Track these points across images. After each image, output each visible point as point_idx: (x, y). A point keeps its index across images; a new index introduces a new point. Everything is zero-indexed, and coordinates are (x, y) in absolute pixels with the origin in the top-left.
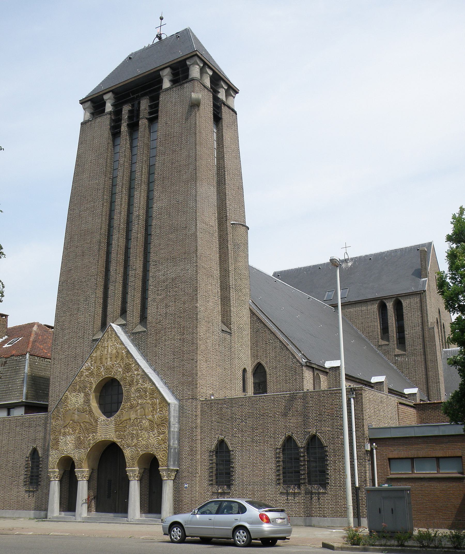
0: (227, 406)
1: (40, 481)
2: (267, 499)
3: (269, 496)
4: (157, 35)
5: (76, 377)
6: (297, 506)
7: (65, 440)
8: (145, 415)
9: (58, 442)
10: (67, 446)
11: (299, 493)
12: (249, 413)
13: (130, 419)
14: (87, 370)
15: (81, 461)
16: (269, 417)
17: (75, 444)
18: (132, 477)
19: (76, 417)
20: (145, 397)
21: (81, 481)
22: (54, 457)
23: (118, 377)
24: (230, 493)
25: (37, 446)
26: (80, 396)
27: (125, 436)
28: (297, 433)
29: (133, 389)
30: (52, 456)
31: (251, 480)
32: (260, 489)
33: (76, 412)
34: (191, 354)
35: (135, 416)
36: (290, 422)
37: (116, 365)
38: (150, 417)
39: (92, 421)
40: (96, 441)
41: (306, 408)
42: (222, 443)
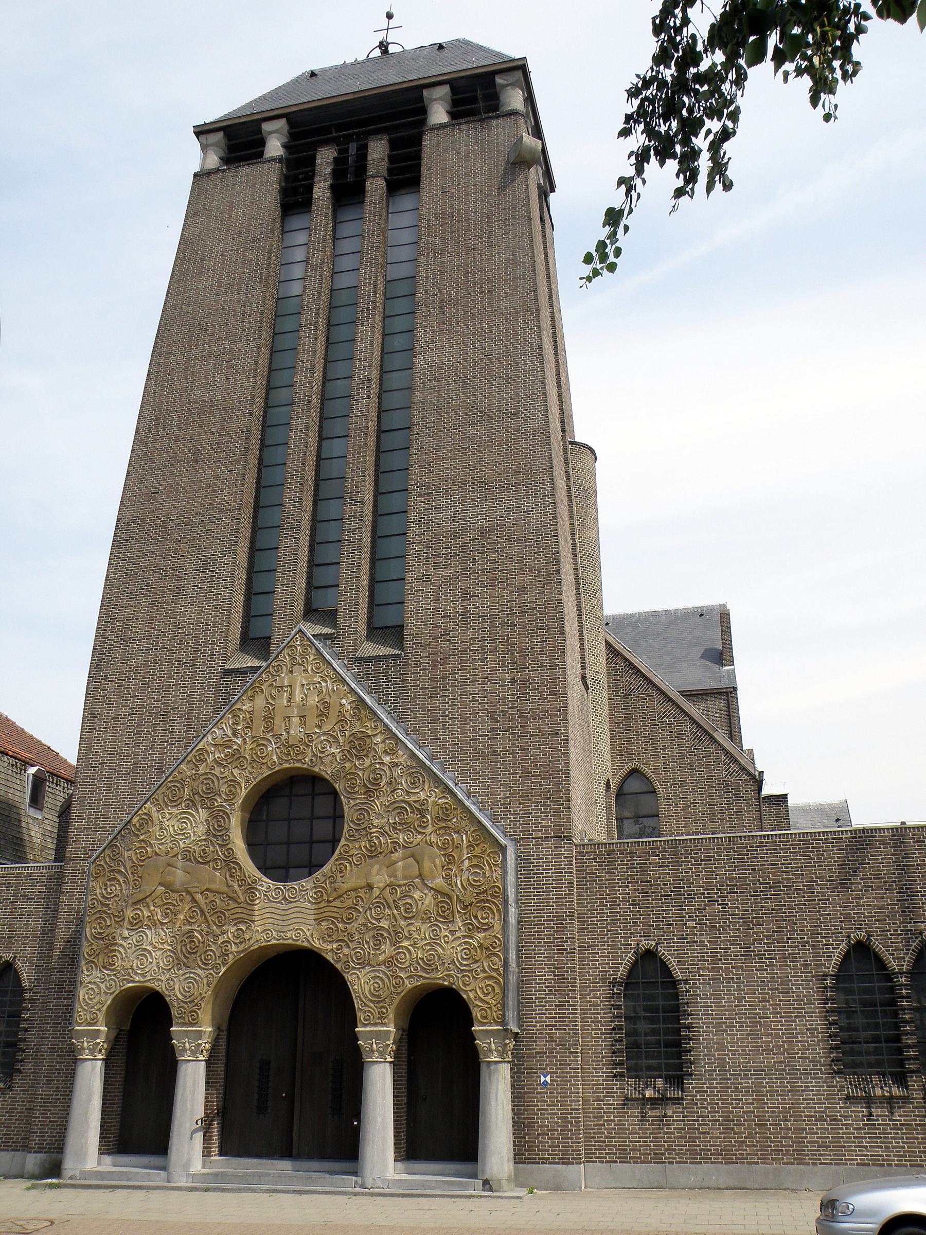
0: (659, 859)
1: (22, 1061)
2: (805, 1116)
3: (811, 1108)
4: (381, 43)
6: (903, 1134)
7: (138, 942)
8: (420, 876)
9: (112, 945)
10: (146, 956)
11: (906, 1099)
12: (731, 879)
13: (370, 887)
15: (193, 1003)
16: (795, 890)
17: (174, 953)
18: (376, 1054)
19: (179, 876)
20: (419, 826)
22: (97, 990)
23: (326, 770)
24: (682, 1099)
25: (15, 957)
26: (193, 816)
27: (351, 935)
28: (881, 935)
29: (378, 804)
30: (90, 986)
31: (749, 1063)
32: (780, 1087)
33: (180, 862)
34: (548, 721)
36: (858, 906)
37: (319, 736)
38: (439, 882)
39: (236, 888)
40: (251, 946)
41: (904, 869)
42: (648, 957)
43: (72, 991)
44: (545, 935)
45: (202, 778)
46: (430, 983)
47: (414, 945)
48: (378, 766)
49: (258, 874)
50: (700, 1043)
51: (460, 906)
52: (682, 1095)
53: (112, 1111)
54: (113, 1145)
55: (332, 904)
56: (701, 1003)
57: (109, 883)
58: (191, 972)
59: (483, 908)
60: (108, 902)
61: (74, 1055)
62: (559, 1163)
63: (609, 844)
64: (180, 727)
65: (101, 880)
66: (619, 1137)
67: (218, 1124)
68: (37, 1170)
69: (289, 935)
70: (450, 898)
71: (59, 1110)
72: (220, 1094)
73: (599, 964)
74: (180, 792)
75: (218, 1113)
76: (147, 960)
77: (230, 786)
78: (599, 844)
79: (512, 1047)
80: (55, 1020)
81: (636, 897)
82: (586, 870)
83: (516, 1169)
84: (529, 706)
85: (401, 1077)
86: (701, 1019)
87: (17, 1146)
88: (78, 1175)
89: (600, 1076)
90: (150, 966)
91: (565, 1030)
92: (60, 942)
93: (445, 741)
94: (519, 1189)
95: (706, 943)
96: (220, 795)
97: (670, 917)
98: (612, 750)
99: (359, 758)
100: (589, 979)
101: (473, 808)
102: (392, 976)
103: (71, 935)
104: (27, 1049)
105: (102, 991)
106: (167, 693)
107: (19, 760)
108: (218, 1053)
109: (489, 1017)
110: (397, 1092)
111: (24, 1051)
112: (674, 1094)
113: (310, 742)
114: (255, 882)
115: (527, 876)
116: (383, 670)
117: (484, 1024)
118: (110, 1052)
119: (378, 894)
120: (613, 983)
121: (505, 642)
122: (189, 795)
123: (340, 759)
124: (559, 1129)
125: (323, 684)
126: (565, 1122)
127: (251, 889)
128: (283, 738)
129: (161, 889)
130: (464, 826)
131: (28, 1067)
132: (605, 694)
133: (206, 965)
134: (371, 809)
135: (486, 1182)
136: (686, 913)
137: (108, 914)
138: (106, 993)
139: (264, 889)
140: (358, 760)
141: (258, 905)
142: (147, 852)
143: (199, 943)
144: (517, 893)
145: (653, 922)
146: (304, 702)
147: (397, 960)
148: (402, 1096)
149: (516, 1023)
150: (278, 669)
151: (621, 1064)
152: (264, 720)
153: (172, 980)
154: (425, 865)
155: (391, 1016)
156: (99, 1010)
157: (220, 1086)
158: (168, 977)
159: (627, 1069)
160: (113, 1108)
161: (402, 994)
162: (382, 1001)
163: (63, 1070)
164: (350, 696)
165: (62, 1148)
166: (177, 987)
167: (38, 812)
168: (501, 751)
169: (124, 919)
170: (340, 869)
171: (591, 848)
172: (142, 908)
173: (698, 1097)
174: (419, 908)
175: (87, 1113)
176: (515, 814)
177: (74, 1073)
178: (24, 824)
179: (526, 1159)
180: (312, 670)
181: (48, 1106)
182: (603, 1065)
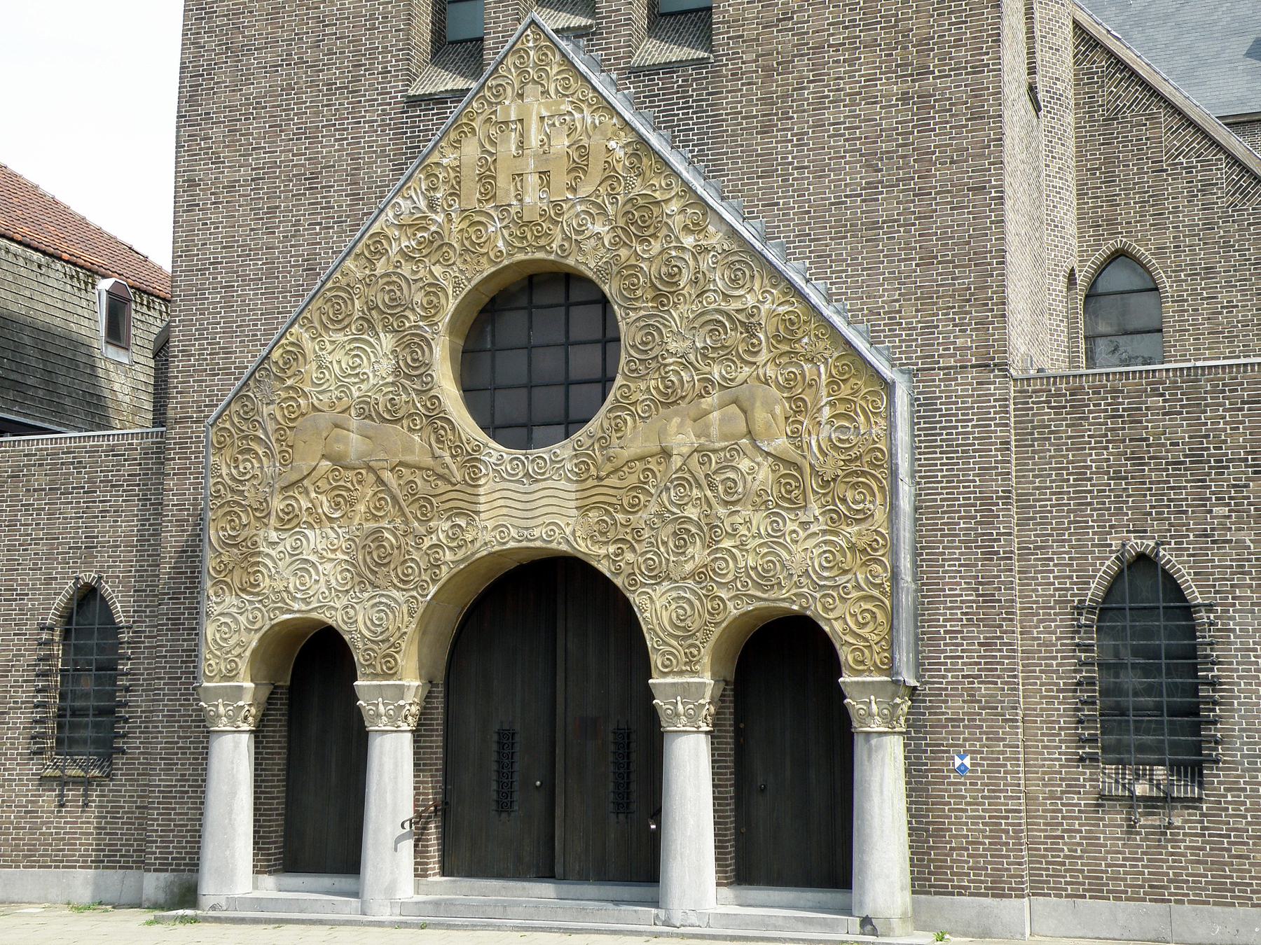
0: (1165, 401)
1: (124, 736)
5: (344, 259)
9: (253, 555)
13: (666, 453)
14: (409, 232)
15: (389, 645)
19: (354, 443)
20: (747, 351)
21: (389, 735)
22: (233, 626)
23: (587, 262)
24: (1200, 800)
25: (100, 578)
26: (372, 346)
27: (638, 531)
30: (223, 620)
33: (354, 422)
37: (573, 206)
38: (781, 444)
39: (448, 459)
43: (194, 629)
44: (960, 529)
47: (742, 546)
48: (674, 253)
49: (482, 437)
50: (1233, 710)
52: (1200, 794)
53: (271, 810)
54: (275, 860)
56: (1236, 643)
58: (383, 595)
59: (855, 486)
60: (241, 488)
61: (204, 726)
62: (986, 895)
63: (1075, 376)
64: (339, 199)
65: (228, 452)
66: (1088, 858)
67: (436, 827)
68: (161, 897)
69: (537, 533)
70: (799, 468)
71: (188, 809)
72: (437, 782)
73: (1055, 577)
74: (346, 307)
75: (436, 811)
77: (428, 294)
78: (1055, 378)
79: (906, 710)
80: (168, 737)
81: (1120, 466)
82: (1032, 421)
83: (914, 902)
84: (934, 140)
85: (725, 755)
86: (1237, 670)
87: (128, 862)
88: (223, 903)
89: (1056, 759)
90: (317, 587)
91: (996, 683)
92: (170, 552)
94: (921, 933)
95: (1248, 543)
96: (413, 310)
97: (1182, 500)
98: (1081, 218)
99: (643, 240)
100: (1037, 602)
101: (838, 321)
102: (707, 596)
103: (187, 541)
104: (130, 717)
105: (243, 627)
106: (314, 140)
107: (82, 267)
108: (432, 719)
109: (868, 662)
110: (719, 779)
111: (126, 721)
112: (1186, 792)
113: (558, 215)
114: (477, 449)
115: (930, 432)
116: (679, 87)
117: (859, 673)
118: (261, 720)
119: (679, 464)
120: (1079, 609)
121: (893, 27)
122: (363, 311)
124: (987, 841)
125: (577, 115)
126: (997, 830)
127: (472, 461)
128: (513, 211)
129: (326, 464)
131: (134, 744)
132: (1070, 119)
134: (665, 326)
135: (866, 921)
136: (1213, 493)
137: (243, 506)
138: (248, 630)
139: (492, 460)
140: (641, 242)
141: (486, 485)
143: (393, 549)
144: (914, 460)
145: (1152, 507)
147: (713, 570)
148: (726, 786)
149: (912, 673)
150: (499, 91)
151: (1092, 740)
152: (480, 180)
153: (353, 607)
155: (706, 660)
156: (239, 656)
157: (437, 770)
159: (1103, 748)
160: (272, 804)
161: (724, 625)
163: (189, 748)
164: (622, 134)
165: (197, 865)
166: (360, 619)
167: (122, 352)
168: (884, 222)
169: (269, 514)
171: (1042, 384)
172: (297, 495)
173: (1230, 798)
174: (748, 486)
175: (231, 812)
176: (910, 329)
177: (207, 753)
178: (101, 373)
179: (930, 886)
180: (557, 91)
181: (171, 803)
182: (1060, 741)
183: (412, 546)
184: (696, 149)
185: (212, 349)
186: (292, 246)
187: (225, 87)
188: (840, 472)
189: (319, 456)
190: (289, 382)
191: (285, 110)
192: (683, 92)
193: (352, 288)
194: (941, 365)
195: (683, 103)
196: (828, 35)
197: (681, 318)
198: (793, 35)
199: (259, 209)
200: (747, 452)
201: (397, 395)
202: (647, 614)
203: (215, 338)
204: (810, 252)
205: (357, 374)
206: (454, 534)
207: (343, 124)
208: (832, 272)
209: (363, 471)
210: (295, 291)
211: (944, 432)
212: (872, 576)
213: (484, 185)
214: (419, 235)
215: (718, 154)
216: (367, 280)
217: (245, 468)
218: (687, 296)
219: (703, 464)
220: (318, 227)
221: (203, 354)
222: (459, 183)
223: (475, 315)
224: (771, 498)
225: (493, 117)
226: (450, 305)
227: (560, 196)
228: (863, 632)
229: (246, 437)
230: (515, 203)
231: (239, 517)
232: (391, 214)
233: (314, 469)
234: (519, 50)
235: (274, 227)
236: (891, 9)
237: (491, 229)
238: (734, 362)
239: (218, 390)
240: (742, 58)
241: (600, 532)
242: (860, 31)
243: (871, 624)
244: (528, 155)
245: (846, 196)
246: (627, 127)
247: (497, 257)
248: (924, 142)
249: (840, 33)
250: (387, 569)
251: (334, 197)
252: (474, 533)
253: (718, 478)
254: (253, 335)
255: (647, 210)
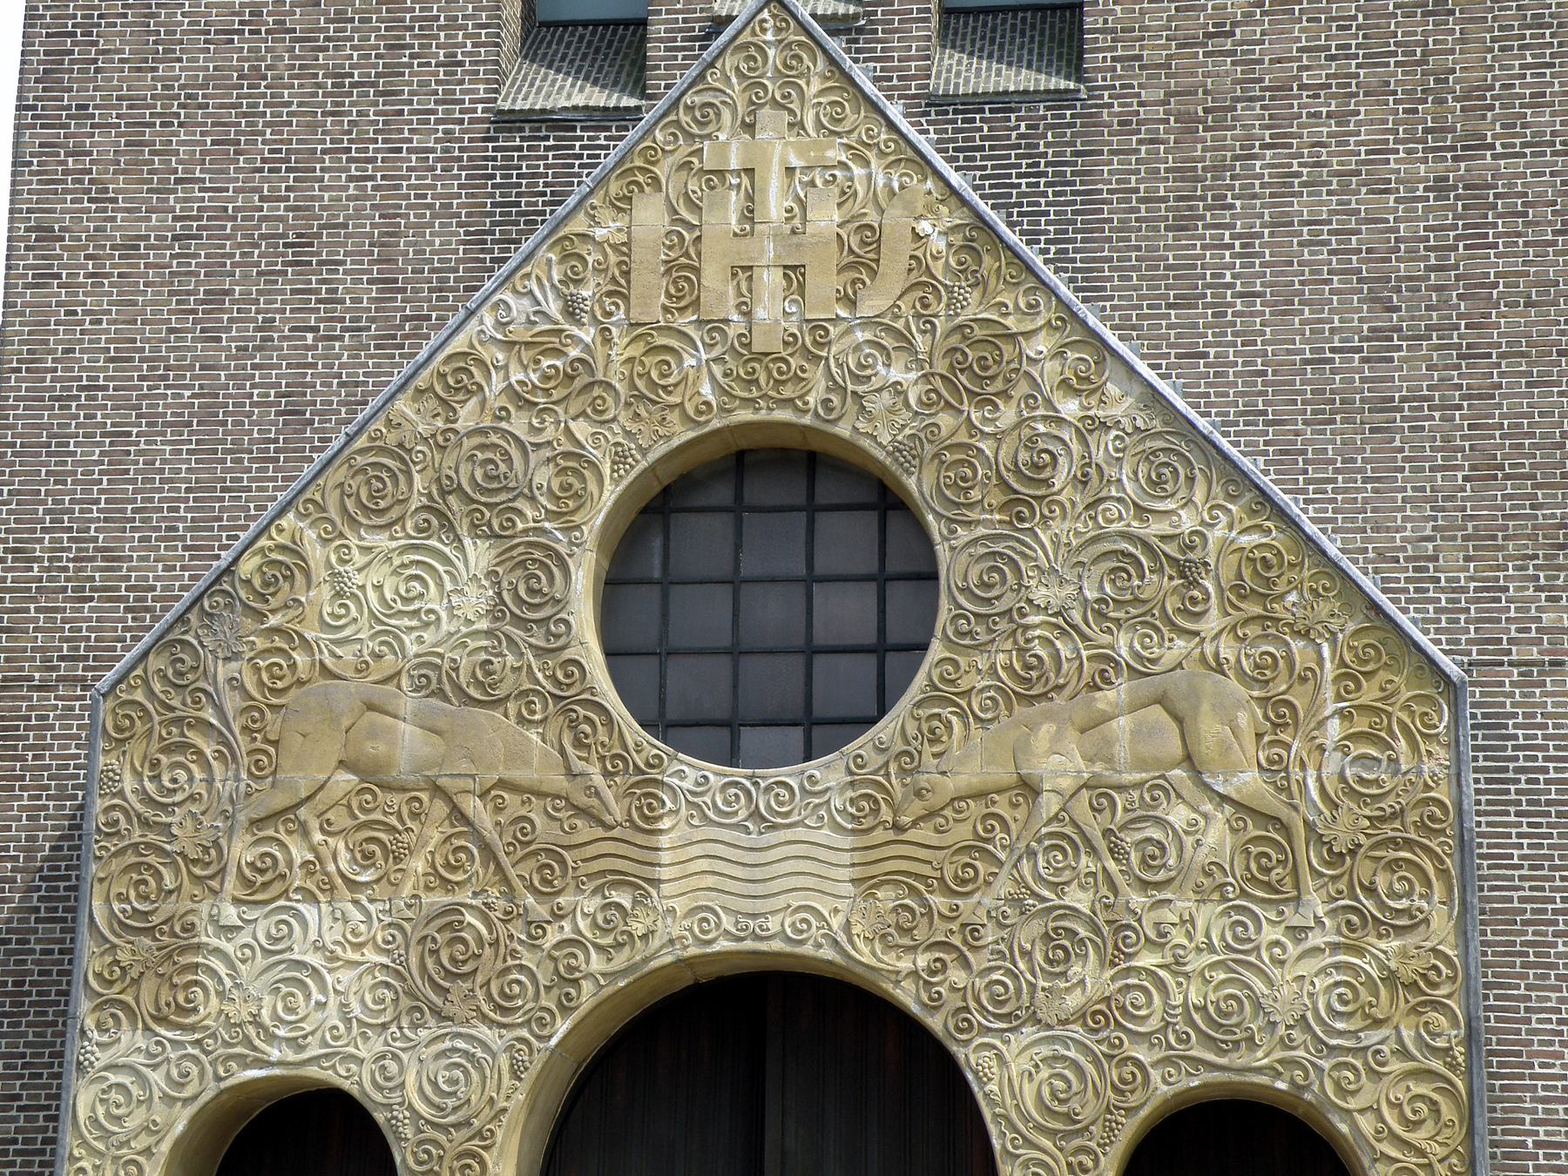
5: (392, 397)
8: (1189, 759)
9: (183, 950)
13: (1029, 788)
14: (526, 355)
22: (136, 1091)
26: (446, 560)
27: (972, 931)
30: (113, 1078)
33: (408, 702)
35: (1082, 764)
37: (849, 331)
38: (1248, 782)
39: (598, 780)
45: (468, 443)
46: (1230, 1083)
48: (1041, 428)
51: (1322, 859)
55: (910, 835)
57: (164, 759)
60: (164, 819)
65: (136, 749)
69: (773, 924)
70: (1285, 829)
76: (308, 996)
77: (563, 471)
84: (1494, 264)
90: (319, 1015)
93: (1222, 362)
96: (532, 499)
102: (1110, 1057)
105: (157, 1094)
106: (304, 172)
113: (821, 345)
116: (1020, 136)
119: (1055, 809)
121: (1418, 63)
122: (430, 496)
123: (920, 401)
125: (858, 171)
128: (732, 332)
129: (346, 780)
130: (1324, 615)
133: (505, 1011)
138: (169, 1100)
139: (687, 784)
141: (673, 830)
142: (293, 666)
146: (797, 222)
150: (707, 115)
152: (668, 271)
153: (395, 1057)
154: (1203, 727)
156: (148, 1152)
158: (379, 1047)
161: (1143, 1113)
162: (1078, 1133)
164: (944, 210)
166: (411, 1080)
169: (222, 871)
170: (932, 731)
172: (283, 836)
176: (1454, 590)
180: (819, 125)
183: (521, 941)
184: (1053, 248)
185: (79, 550)
186: (254, 366)
187: (121, 61)
188: (1362, 839)
189: (334, 763)
190: (273, 621)
191: (245, 115)
192: (1028, 146)
193: (409, 451)
194: (1514, 657)
195: (1029, 166)
196: (1300, 69)
197: (1056, 544)
198: (1234, 63)
199: (188, 293)
200: (1184, 793)
201: (496, 655)
202: (993, 1087)
203: (88, 530)
204: (1266, 443)
205: (416, 612)
206: (607, 921)
207: (366, 150)
208: (1308, 482)
209: (424, 796)
210: (260, 451)
211: (1523, 778)
212: (1429, 1032)
213: (675, 282)
214: (546, 363)
215: (1094, 260)
216: (440, 439)
217: (174, 781)
218: (1068, 505)
219: (1100, 811)
220: (310, 336)
221: (60, 559)
222: (626, 274)
223: (633, 516)
224: (1231, 880)
225: (695, 160)
226: (606, 494)
227: (825, 311)
228: (1417, 1137)
229: (178, 721)
230: (735, 317)
231: (159, 876)
232: (489, 321)
233: (321, 788)
234: (746, 46)
235: (218, 330)
236: (1415, 33)
237: (689, 361)
238: (1157, 630)
239: (89, 629)
240: (1138, 96)
241: (899, 928)
242: (1359, 66)
243: (1430, 1123)
244: (762, 233)
245: (1333, 350)
246: (953, 200)
247: (699, 412)
248: (1477, 266)
249: (1321, 67)
250: (468, 985)
251: (344, 282)
252: (649, 921)
253: (1130, 838)
254: (169, 529)
255: (990, 347)
